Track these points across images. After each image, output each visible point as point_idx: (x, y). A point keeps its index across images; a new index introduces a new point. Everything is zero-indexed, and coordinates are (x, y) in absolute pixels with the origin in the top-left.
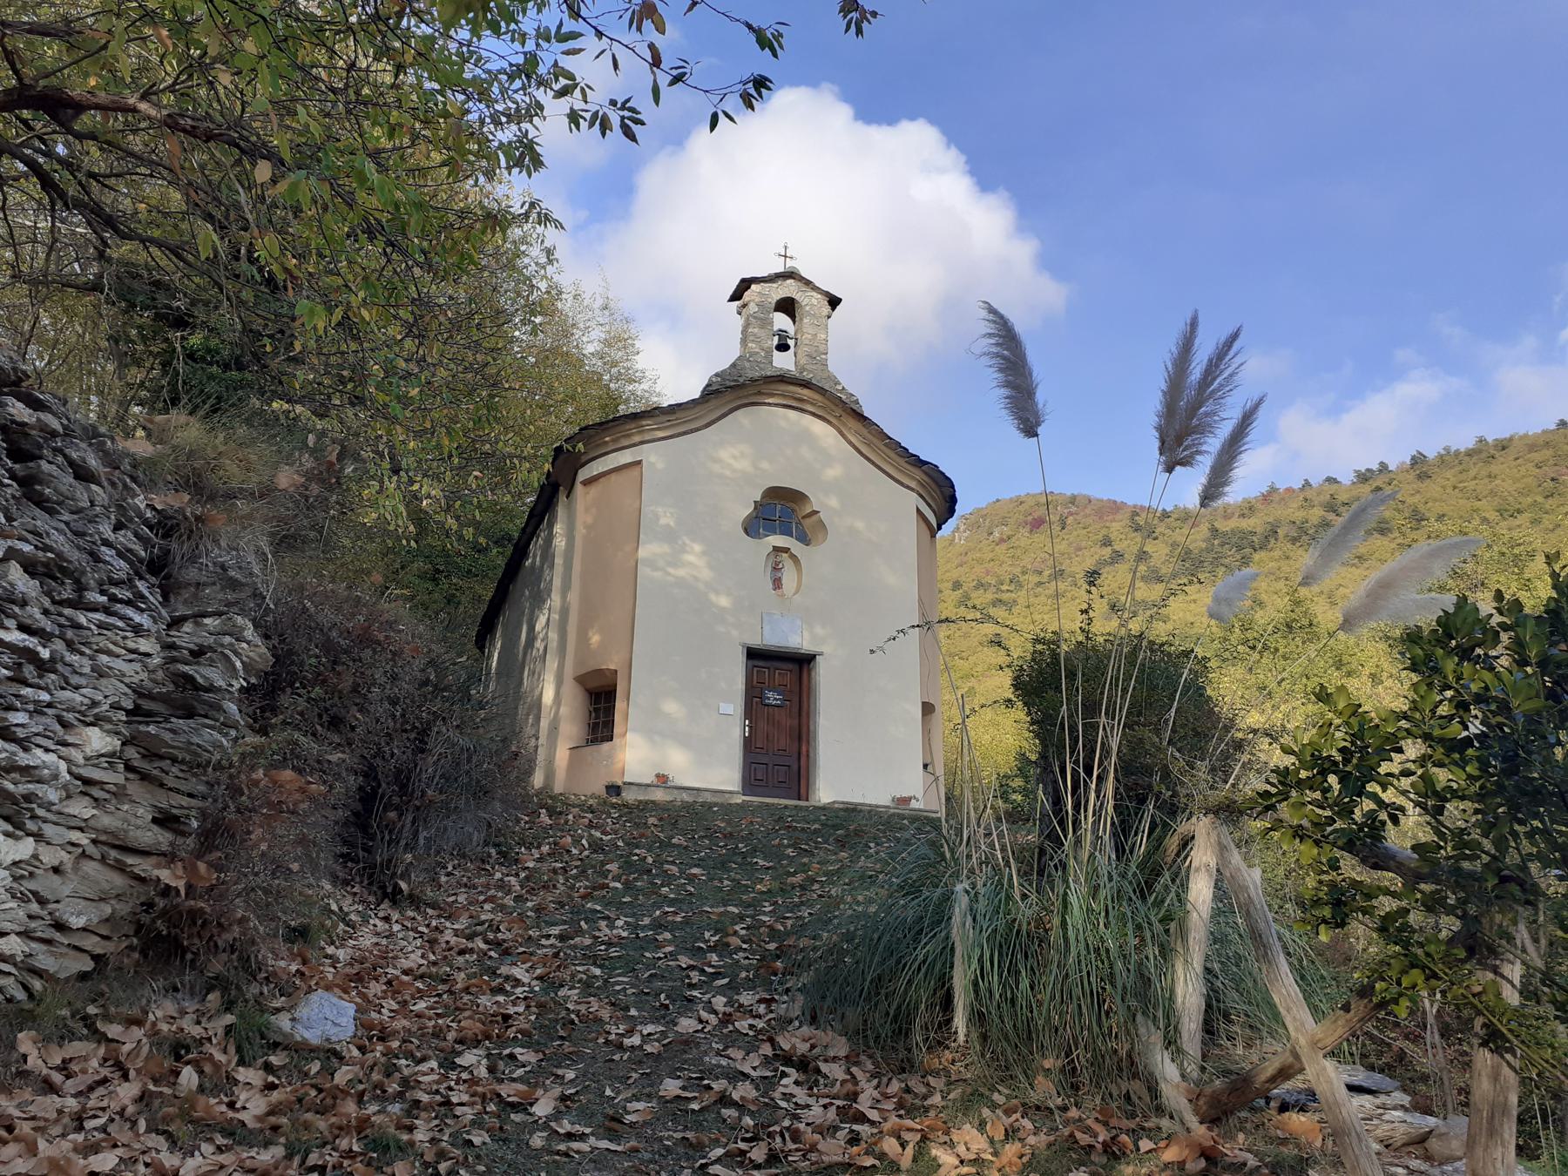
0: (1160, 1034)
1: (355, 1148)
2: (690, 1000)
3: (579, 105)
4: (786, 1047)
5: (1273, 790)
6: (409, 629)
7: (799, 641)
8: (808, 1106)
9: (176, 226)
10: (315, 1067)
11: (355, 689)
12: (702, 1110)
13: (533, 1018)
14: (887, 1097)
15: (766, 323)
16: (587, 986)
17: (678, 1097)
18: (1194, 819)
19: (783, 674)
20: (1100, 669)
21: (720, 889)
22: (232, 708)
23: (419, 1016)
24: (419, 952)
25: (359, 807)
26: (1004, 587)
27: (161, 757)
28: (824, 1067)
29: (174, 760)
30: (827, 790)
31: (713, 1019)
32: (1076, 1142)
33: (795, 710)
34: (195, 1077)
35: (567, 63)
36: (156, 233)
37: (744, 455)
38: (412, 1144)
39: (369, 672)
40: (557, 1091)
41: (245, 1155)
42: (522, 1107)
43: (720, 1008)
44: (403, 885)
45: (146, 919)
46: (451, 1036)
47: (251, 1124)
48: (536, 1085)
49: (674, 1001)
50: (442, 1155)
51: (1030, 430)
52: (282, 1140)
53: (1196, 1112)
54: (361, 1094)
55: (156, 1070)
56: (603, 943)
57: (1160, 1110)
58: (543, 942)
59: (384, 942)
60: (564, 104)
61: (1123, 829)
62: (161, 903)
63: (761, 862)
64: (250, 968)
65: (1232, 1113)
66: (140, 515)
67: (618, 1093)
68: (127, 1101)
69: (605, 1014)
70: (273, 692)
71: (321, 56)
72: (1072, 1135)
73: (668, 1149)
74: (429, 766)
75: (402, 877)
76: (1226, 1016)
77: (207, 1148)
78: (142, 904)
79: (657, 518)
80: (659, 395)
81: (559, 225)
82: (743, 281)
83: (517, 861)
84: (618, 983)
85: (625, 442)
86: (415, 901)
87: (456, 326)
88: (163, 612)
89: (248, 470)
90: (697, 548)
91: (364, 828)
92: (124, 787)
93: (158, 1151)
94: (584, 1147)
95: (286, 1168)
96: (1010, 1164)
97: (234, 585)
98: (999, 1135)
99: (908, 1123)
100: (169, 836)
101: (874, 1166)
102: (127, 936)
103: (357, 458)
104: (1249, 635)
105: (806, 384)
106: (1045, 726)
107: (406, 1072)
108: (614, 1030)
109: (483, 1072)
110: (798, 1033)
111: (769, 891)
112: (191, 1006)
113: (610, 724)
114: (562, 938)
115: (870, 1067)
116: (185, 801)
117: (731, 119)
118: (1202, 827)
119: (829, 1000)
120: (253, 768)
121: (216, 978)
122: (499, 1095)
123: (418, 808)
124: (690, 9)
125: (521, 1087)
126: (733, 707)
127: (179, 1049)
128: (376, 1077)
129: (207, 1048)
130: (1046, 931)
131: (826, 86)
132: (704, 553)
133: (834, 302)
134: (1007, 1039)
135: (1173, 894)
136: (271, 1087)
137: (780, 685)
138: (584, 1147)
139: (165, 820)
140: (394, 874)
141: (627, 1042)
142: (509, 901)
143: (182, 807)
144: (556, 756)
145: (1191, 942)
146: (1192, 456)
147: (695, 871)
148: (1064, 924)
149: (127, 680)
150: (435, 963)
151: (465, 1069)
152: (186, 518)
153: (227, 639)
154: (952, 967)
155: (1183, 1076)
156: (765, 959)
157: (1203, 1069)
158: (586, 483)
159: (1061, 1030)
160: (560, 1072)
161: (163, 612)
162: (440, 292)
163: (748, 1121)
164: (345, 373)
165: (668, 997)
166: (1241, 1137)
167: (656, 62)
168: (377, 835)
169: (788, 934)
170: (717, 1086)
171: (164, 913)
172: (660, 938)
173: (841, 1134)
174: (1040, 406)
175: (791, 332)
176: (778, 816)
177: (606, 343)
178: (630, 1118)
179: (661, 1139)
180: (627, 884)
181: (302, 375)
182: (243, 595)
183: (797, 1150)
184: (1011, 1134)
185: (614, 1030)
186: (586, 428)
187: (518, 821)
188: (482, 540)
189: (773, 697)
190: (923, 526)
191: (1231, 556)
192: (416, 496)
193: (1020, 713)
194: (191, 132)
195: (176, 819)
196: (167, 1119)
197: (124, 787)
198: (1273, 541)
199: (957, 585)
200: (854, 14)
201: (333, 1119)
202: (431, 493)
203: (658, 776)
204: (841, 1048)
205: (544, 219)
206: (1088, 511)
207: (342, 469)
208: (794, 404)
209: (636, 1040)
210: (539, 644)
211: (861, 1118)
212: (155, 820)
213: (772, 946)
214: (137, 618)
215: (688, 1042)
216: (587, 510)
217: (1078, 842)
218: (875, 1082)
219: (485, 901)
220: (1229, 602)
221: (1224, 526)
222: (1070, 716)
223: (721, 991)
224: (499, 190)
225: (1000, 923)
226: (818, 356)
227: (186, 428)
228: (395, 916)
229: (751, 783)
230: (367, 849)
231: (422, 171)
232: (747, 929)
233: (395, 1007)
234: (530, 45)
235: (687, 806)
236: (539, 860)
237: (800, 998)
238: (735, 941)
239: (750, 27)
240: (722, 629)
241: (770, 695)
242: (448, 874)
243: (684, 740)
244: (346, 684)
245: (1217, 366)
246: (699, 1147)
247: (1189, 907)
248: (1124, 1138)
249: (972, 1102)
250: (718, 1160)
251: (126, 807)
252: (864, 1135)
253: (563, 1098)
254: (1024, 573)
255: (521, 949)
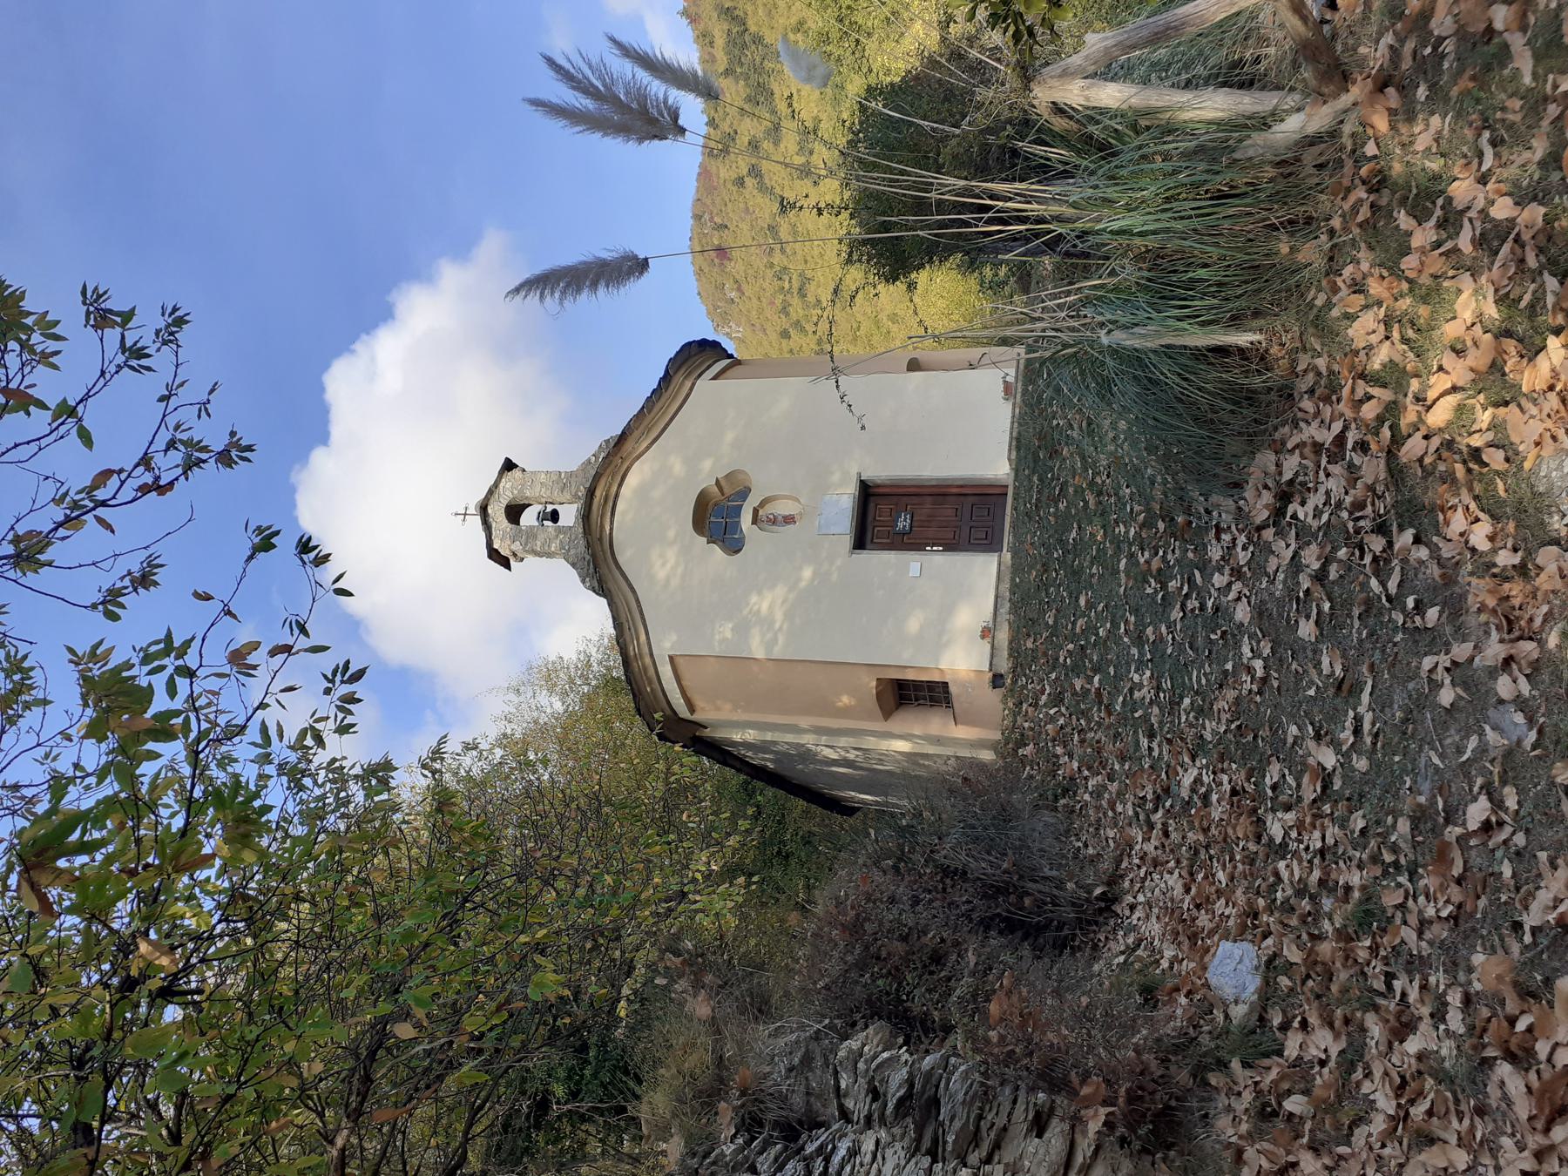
0: (1254, 135)
1: (1368, 943)
2: (1217, 609)
3: (331, 725)
4: (1266, 514)
5: (1012, 28)
6: (844, 885)
7: (844, 500)
8: (1328, 493)
9: (450, 1110)
10: (1284, 981)
11: (904, 939)
12: (1330, 600)
13: (1234, 766)
14: (1318, 413)
15: (531, 534)
16: (1202, 712)
17: (1317, 623)
18: (1035, 102)
19: (880, 511)
20: (878, 196)
21: (1101, 576)
22: (928, 1061)
23: (1232, 878)
24: (1166, 876)
25: (1019, 934)
26: (787, 286)
27: (978, 1128)
28: (1287, 476)
29: (980, 1117)
30: (996, 466)
31: (1237, 586)
32: (1367, 221)
33: (915, 500)
34: (1293, 1098)
35: (291, 734)
36: (461, 1127)
37: (661, 554)
38: (1363, 888)
39: (887, 925)
40: (1311, 744)
41: (1374, 1051)
42: (1327, 779)
43: (1225, 579)
44: (1098, 891)
45: (1137, 1145)
46: (1252, 847)
47: (1343, 1044)
48: (1304, 764)
49: (1218, 626)
50: (1376, 859)
51: (642, 265)
52: (1359, 1014)
53: (1336, 96)
54: (1313, 937)
55: (1289, 1135)
56: (1157, 695)
57: (1334, 134)
58: (1156, 754)
59: (1155, 910)
60: (330, 738)
61: (1043, 171)
62: (1121, 1130)
63: (1073, 534)
64: (1185, 1044)
65: (1337, 59)
66: (741, 1149)
67: (1313, 683)
68: (1319, 1165)
69: (1231, 694)
70: (908, 1019)
71: (286, 972)
72: (1360, 225)
73: (1370, 635)
74: (980, 866)
75: (1090, 892)
76: (1239, 64)
77: (1367, 1087)
78: (1122, 1147)
79: (725, 640)
80: (602, 637)
81: (443, 740)
82: (490, 557)
83: (1072, 779)
84: (1199, 681)
85: (651, 671)
86: (1114, 880)
87: (540, 838)
88: (835, 1127)
89: (694, 1044)
90: (754, 599)
91: (1040, 929)
92: (1007, 1165)
93: (1370, 1135)
94: (1368, 718)
95: (1387, 1010)
96: (1389, 289)
97: (807, 1060)
98: (1359, 300)
99: (1346, 392)
100: (1055, 1122)
101: (1391, 428)
102: (1153, 1164)
103: (677, 937)
104: (834, 35)
105: (591, 493)
106: (932, 252)
107: (1289, 892)
108: (1247, 686)
109: (1290, 817)
110: (1251, 502)
111: (1103, 527)
112: (1222, 1101)
113: (931, 686)
114: (1151, 736)
115: (1287, 429)
116: (1020, 1107)
117: (341, 576)
118: (1043, 95)
119: (1219, 470)
120: (987, 1041)
121: (1195, 1077)
122: (1314, 801)
123: (1021, 877)
124: (234, 617)
125: (1306, 779)
126: (913, 563)
127: (1266, 1113)
128: (1294, 922)
129: (1265, 1085)
130: (1148, 251)
131: (293, 478)
132: (760, 593)
133: (509, 466)
134: (1259, 290)
135: (1112, 123)
136: (1304, 1025)
137: (892, 516)
138: (1368, 718)
139: (1039, 1126)
140: (1088, 900)
141: (1260, 673)
142: (1114, 787)
143: (1027, 1110)
144: (963, 738)
145: (1160, 104)
146: (668, 108)
147: (1082, 602)
148: (1141, 234)
149: (903, 1163)
150: (1178, 862)
151: (1286, 834)
152: (743, 1106)
153: (861, 1065)
154: (1185, 347)
155: (1299, 110)
156: (1173, 532)
157: (1292, 89)
158: (692, 710)
159: (1250, 236)
160: (1290, 740)
161: (835, 1127)
162: (509, 858)
163: (1342, 553)
164: (588, 946)
165: (1214, 632)
166: (1363, 50)
167: (287, 649)
168: (1050, 919)
169: (1148, 510)
170: (1306, 583)
171: (1132, 1128)
172: (1152, 638)
173: (1357, 460)
174: (615, 255)
175: (539, 508)
176: (1025, 517)
177: (551, 691)
178: (1338, 672)
179: (1361, 641)
180: (1096, 670)
181: (593, 988)
182: (818, 1051)
183: (1373, 504)
184: (1358, 287)
185: (1247, 686)
186: (638, 711)
187: (1031, 777)
188: (750, 812)
189: (903, 523)
190: (729, 373)
191: (753, 54)
192: (708, 876)
193: (922, 277)
194: (363, 1097)
195: (1038, 1115)
196: (1337, 1126)
197: (1007, 1165)
198: (737, 12)
199: (785, 334)
200: (234, 453)
201: (1338, 964)
202: (704, 862)
203: (983, 637)
204: (1267, 458)
205: (437, 754)
206: (709, 202)
207: (688, 951)
208: (610, 504)
209: (1258, 664)
210: (851, 756)
211: (1340, 440)
212: (1039, 1136)
213: (1161, 526)
214: (842, 1152)
215: (1260, 612)
216: (718, 709)
217: (1058, 219)
218: (1302, 424)
219: (1113, 810)
220: (811, 68)
221: (722, 62)
222: (929, 227)
223: (1207, 578)
224: (406, 795)
225: (1142, 298)
226: (563, 481)
227: (654, 1104)
228: (1129, 899)
229: (989, 543)
230: (1060, 928)
231: (394, 873)
232: (1143, 550)
233: (1223, 901)
234: (270, 770)
235: (1014, 609)
236: (1071, 757)
237: (1214, 498)
238: (1156, 564)
239: (251, 558)
240: (834, 577)
241: (900, 525)
242: (1086, 846)
243: (947, 611)
244: (900, 947)
245: (579, 82)
246: (1369, 604)
247: (1124, 106)
248: (1364, 171)
249: (1323, 327)
250: (1383, 584)
251: (1027, 1163)
252: (1358, 437)
253: (1318, 737)
254: (772, 265)
255: (1164, 776)
